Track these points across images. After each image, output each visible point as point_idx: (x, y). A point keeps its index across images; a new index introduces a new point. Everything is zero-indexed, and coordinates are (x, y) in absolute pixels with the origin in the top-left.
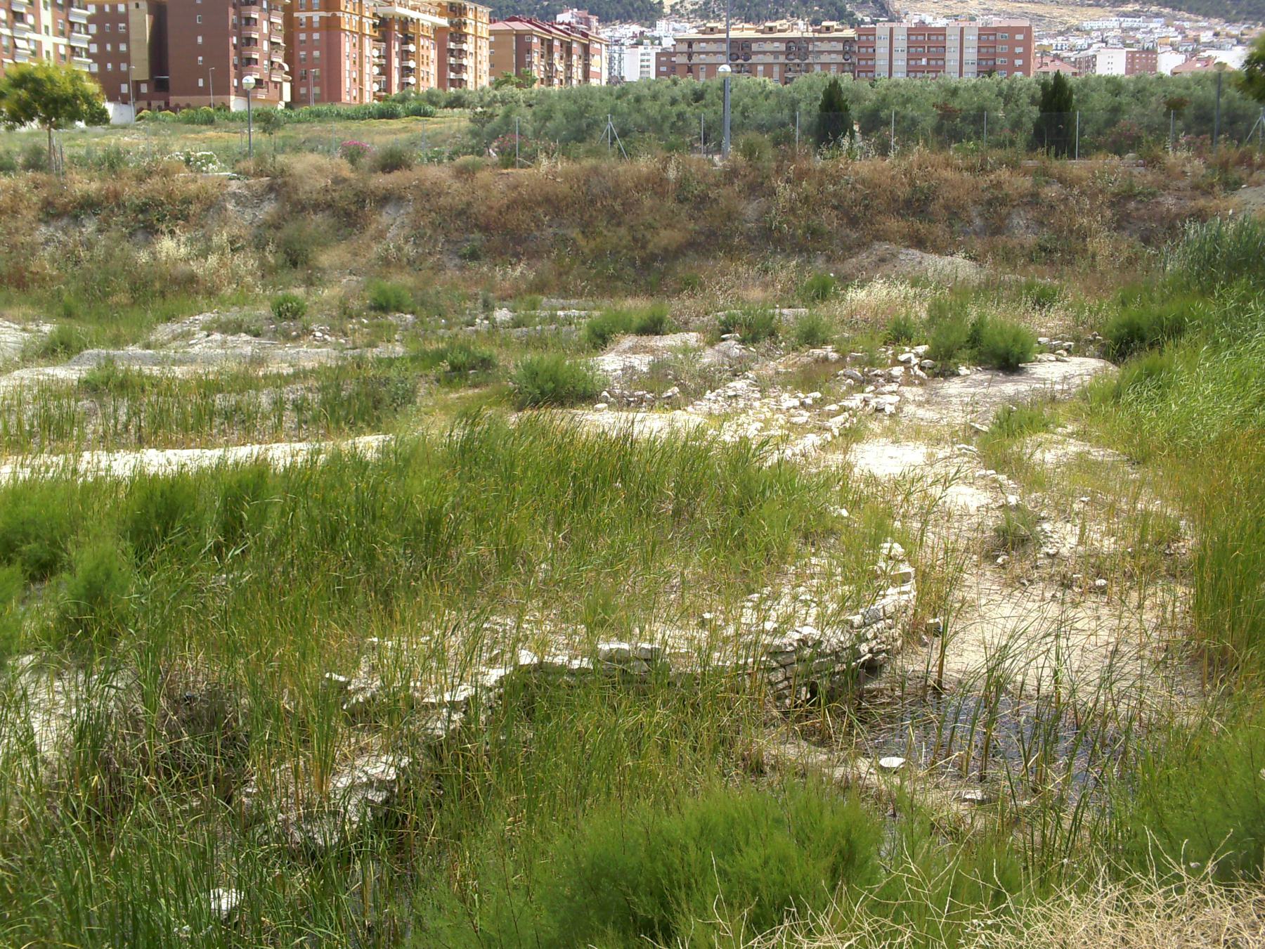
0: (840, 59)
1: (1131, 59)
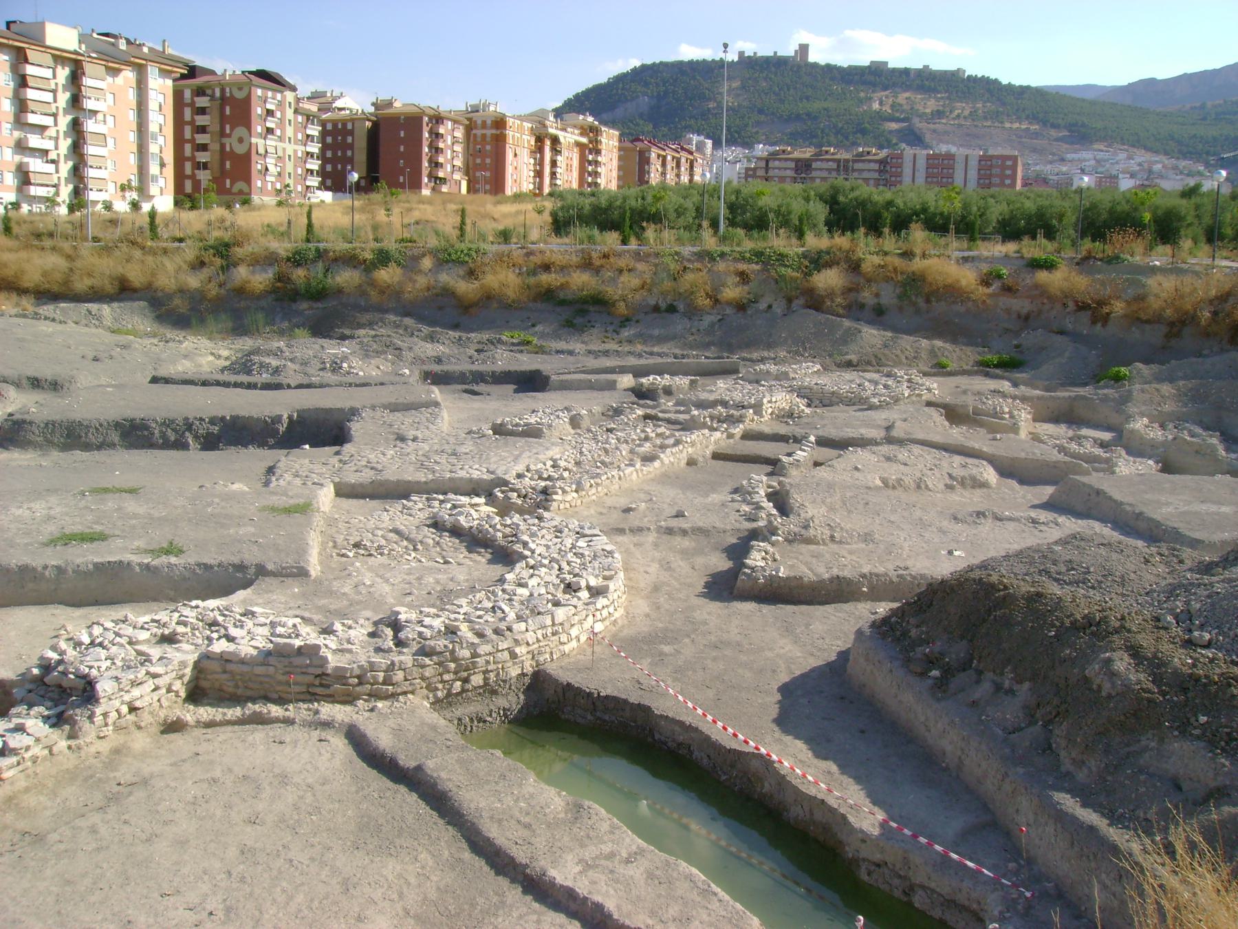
0: (876, 175)
1: (1099, 183)
